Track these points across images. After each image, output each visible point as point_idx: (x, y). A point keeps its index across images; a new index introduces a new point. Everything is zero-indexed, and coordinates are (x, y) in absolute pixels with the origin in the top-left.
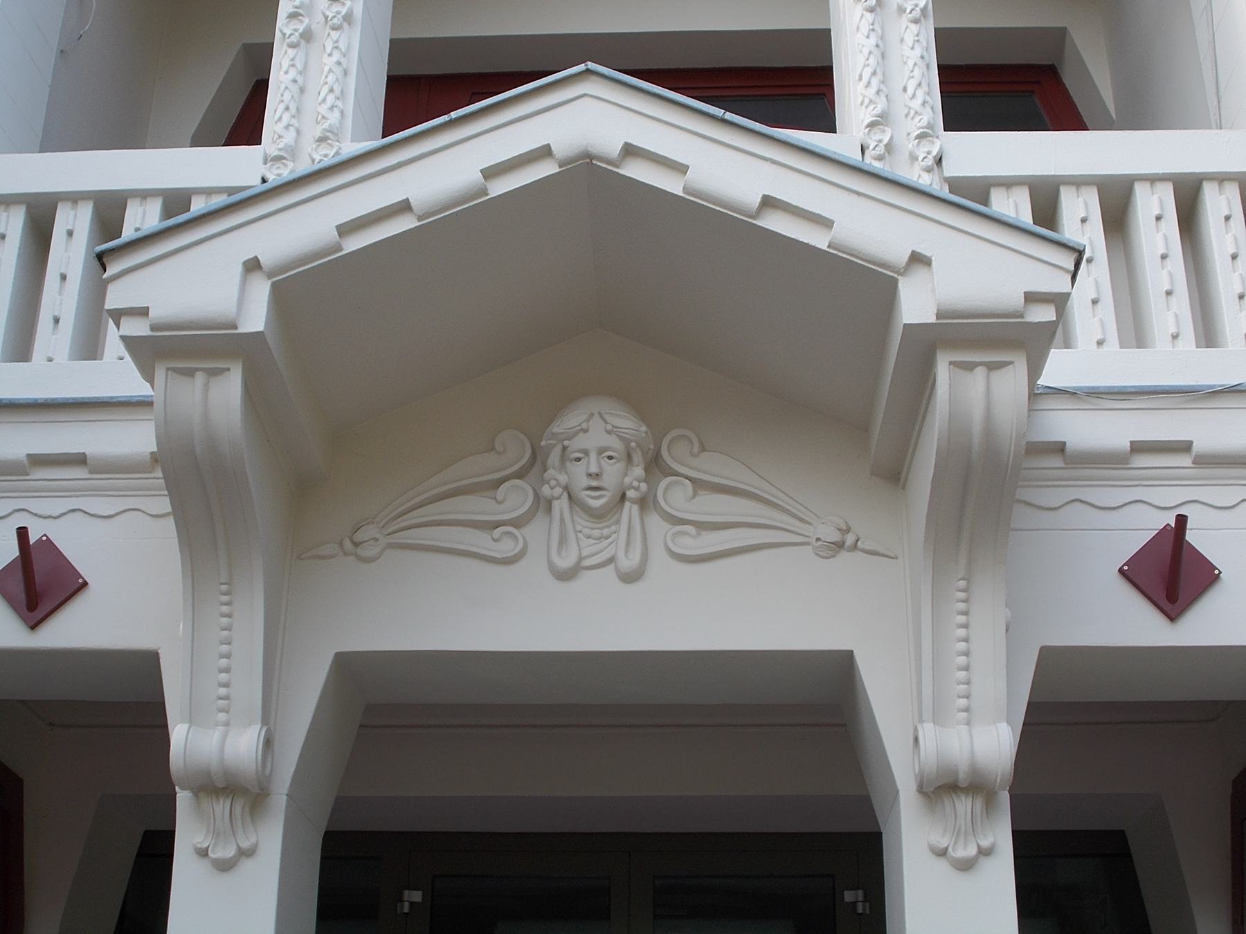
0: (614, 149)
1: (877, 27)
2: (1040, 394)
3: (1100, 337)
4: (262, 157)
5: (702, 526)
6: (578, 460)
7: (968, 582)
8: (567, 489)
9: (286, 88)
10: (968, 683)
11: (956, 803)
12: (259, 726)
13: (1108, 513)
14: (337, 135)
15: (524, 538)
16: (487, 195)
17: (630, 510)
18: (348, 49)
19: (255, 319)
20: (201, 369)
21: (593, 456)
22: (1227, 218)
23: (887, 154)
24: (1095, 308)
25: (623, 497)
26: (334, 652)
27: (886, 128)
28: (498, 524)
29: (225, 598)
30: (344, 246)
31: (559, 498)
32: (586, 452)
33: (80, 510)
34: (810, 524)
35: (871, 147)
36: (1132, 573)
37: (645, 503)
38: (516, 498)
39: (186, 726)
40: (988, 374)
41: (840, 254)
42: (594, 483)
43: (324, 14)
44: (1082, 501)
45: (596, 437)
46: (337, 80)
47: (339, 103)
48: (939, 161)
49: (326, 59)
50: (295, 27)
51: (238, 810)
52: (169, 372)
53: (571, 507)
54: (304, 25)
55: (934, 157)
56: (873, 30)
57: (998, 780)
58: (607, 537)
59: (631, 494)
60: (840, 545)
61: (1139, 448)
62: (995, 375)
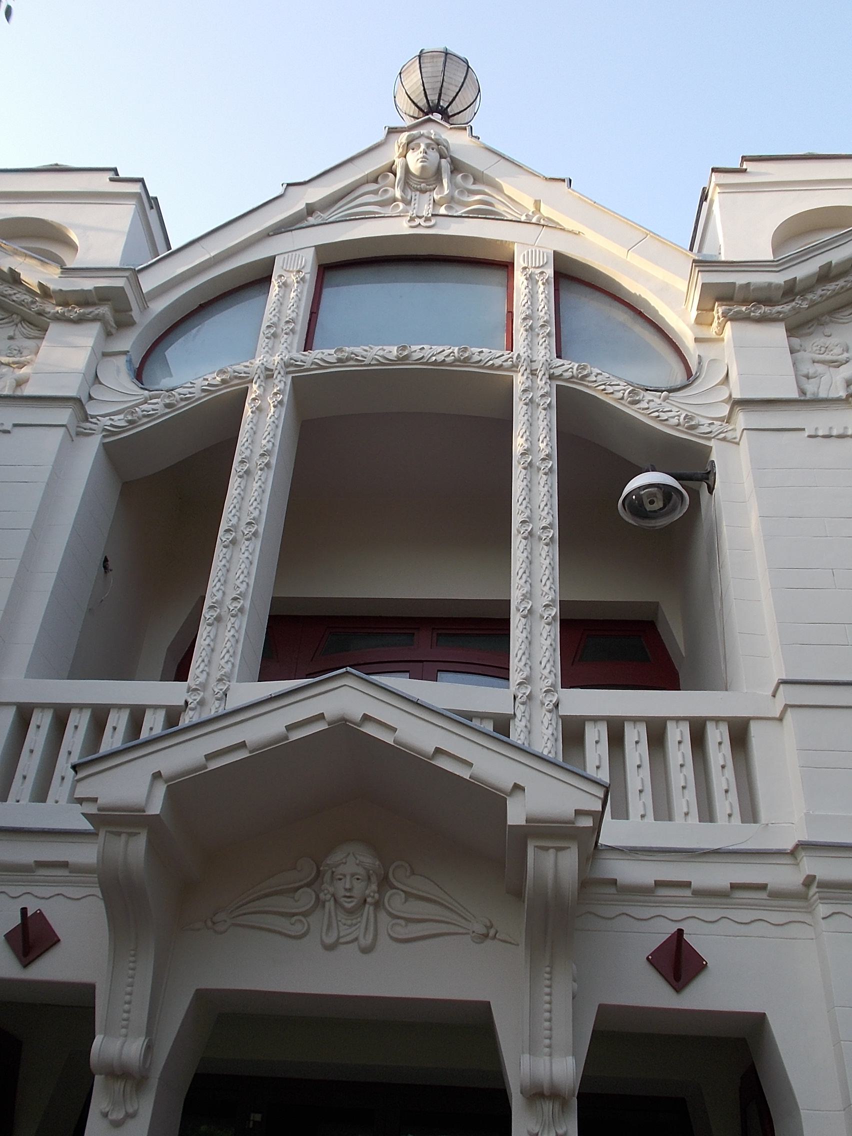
0: (358, 717)
1: (527, 627)
2: (603, 850)
3: (643, 813)
4: (186, 688)
5: (409, 920)
6: (340, 879)
7: (552, 968)
8: (333, 895)
9: (204, 649)
10: (551, 1029)
11: (543, 1106)
12: (144, 1038)
13: (640, 922)
14: (229, 677)
15: (309, 925)
16: (288, 740)
17: (369, 909)
18: (240, 627)
19: (155, 808)
20: (124, 832)
21: (348, 877)
22: (720, 743)
23: (528, 701)
24: (641, 794)
25: (365, 901)
26: (195, 988)
27: (528, 686)
28: (294, 915)
29: (132, 959)
30: (208, 766)
31: (329, 901)
32: (345, 876)
33: (61, 894)
34: (470, 922)
35: (519, 697)
36: (655, 960)
37: (377, 905)
38: (306, 899)
39: (102, 1036)
40: (556, 854)
41: (476, 782)
42: (348, 894)
43: (228, 607)
44: (627, 915)
45: (350, 867)
46: (232, 645)
47: (231, 659)
48: (557, 706)
49: (227, 634)
50: (212, 614)
51: (128, 1089)
52: (108, 834)
53: (336, 908)
54: (217, 613)
55: (553, 704)
56: (525, 628)
57: (567, 1092)
58: (356, 924)
59: (369, 900)
60: (486, 936)
61: (659, 884)
62: (560, 854)
